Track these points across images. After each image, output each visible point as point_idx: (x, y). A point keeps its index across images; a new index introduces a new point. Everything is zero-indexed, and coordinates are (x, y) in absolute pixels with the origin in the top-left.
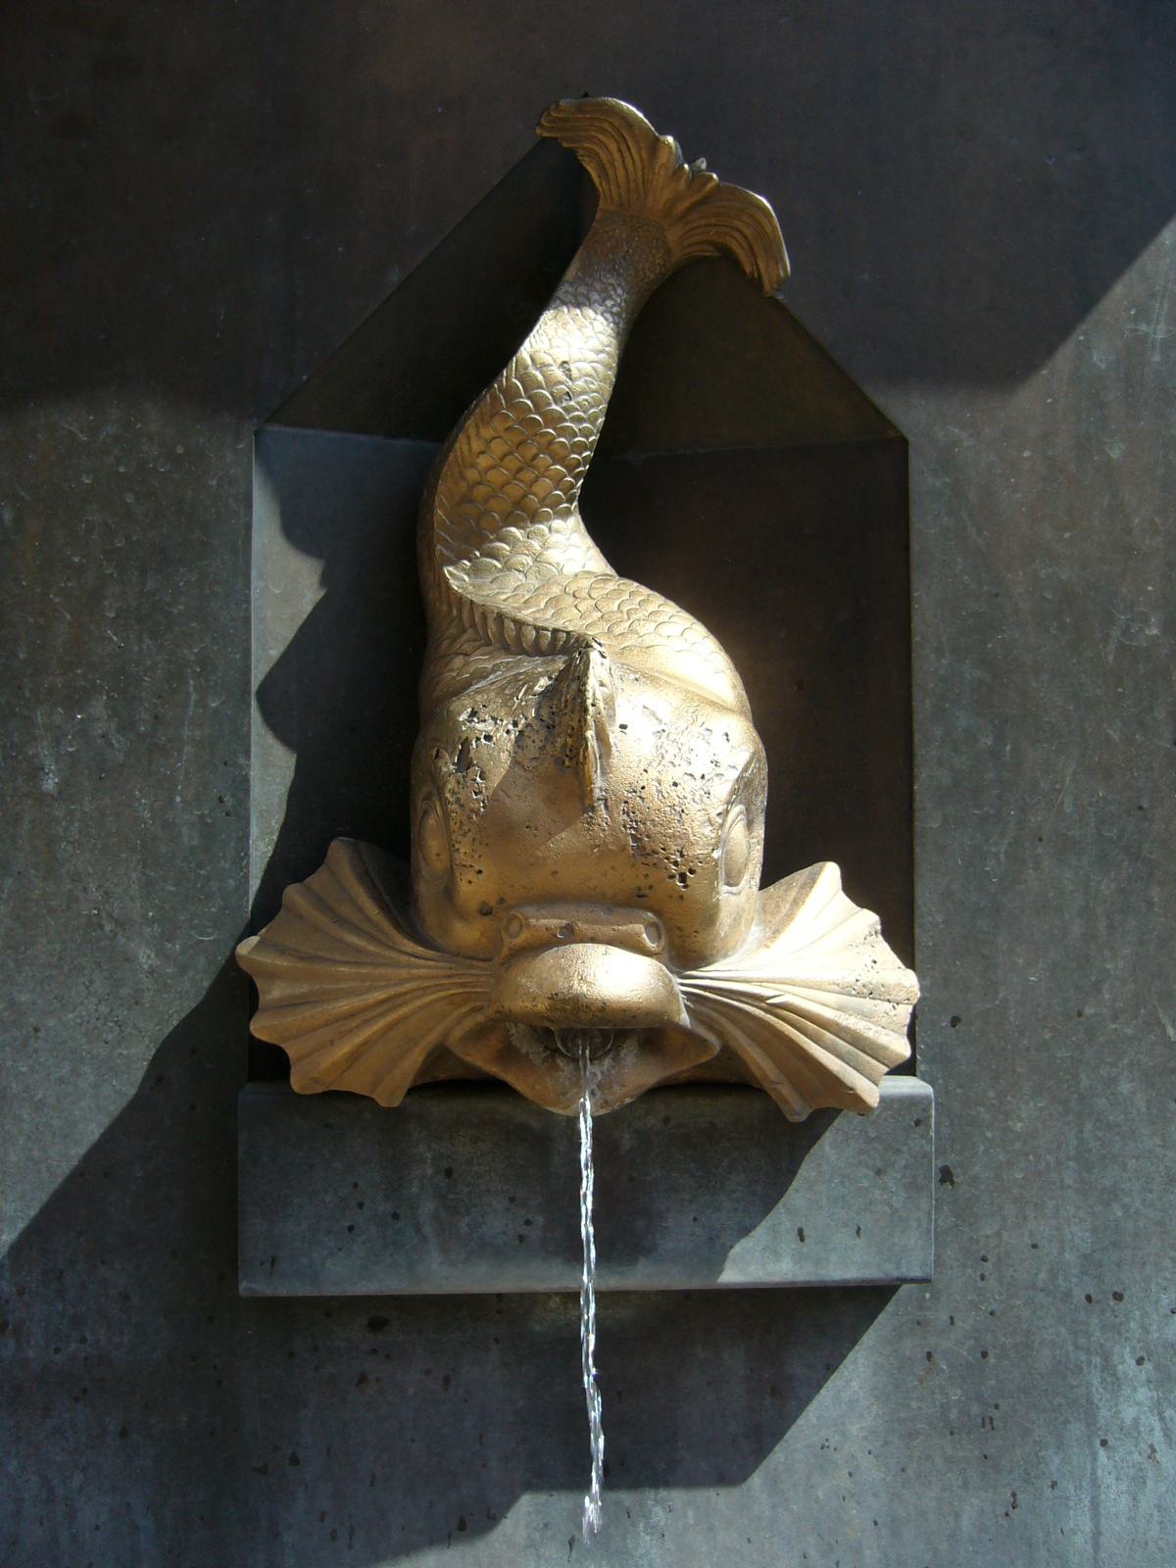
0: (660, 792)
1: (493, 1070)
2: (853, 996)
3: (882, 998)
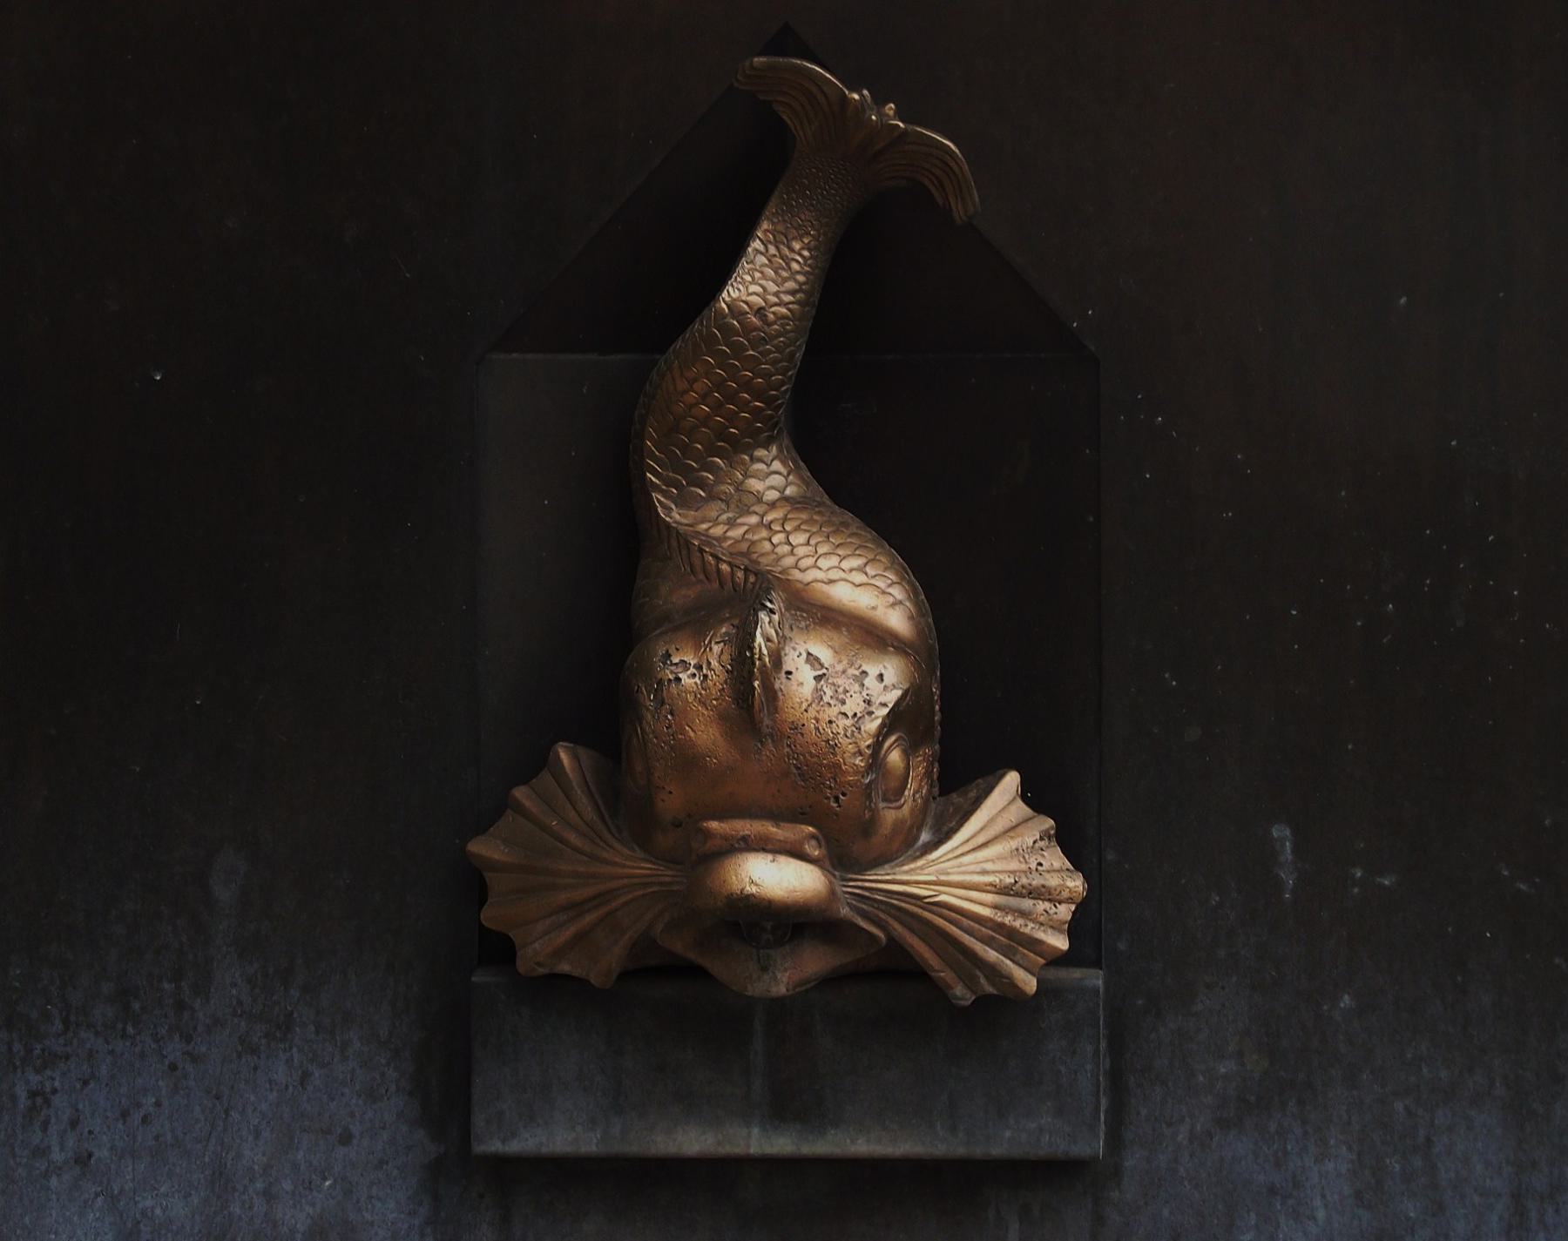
0: (817, 729)
1: (693, 956)
2: (1011, 895)
3: (1042, 897)
